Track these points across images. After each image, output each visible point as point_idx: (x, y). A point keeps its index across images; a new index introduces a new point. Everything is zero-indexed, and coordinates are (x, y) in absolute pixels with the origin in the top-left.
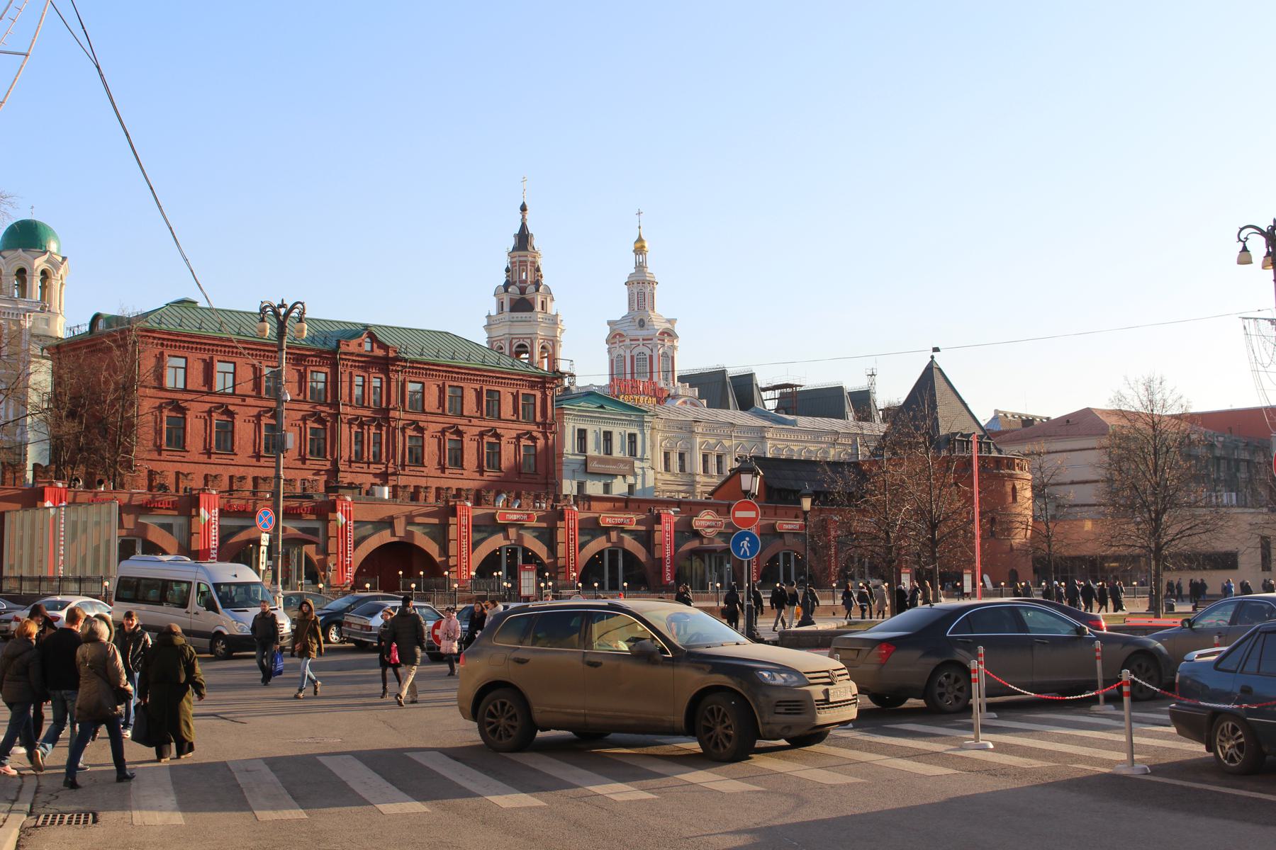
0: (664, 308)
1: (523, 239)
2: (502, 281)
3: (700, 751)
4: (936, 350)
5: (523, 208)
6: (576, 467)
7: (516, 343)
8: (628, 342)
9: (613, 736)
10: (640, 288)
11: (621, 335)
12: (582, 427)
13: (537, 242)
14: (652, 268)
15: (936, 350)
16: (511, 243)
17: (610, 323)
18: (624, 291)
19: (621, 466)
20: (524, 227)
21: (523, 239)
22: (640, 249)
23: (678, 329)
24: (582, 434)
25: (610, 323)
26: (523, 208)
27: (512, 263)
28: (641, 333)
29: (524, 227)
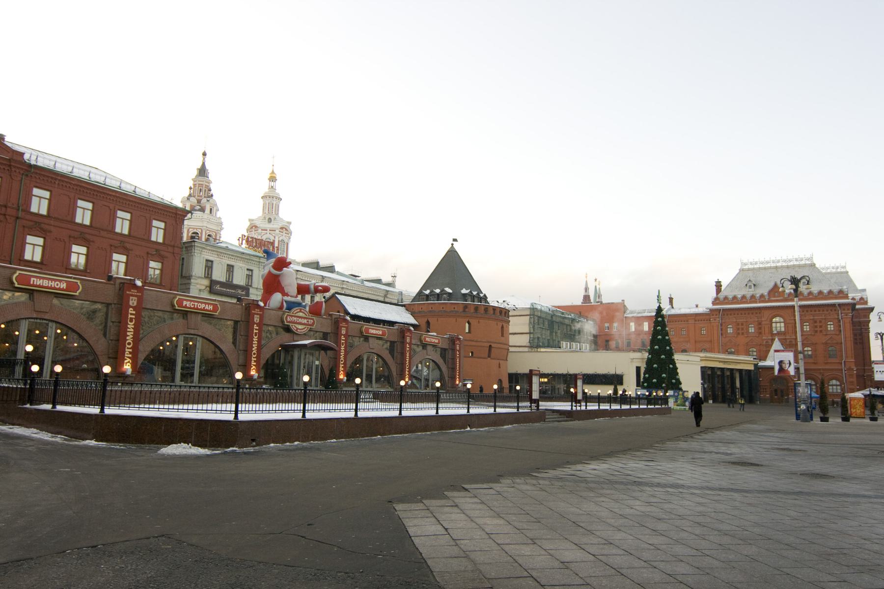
0: (285, 213)
1: (203, 171)
2: (187, 194)
3: (399, 507)
4: (455, 240)
5: (204, 154)
6: (204, 287)
7: (191, 231)
8: (260, 231)
9: (639, 513)
10: (271, 201)
11: (256, 227)
12: (211, 258)
13: (212, 176)
14: (281, 188)
15: (455, 240)
16: (195, 173)
17: (250, 220)
18: (261, 202)
19: (239, 291)
20: (204, 164)
21: (203, 171)
22: (273, 179)
23: (292, 227)
24: (209, 265)
25: (250, 220)
26: (204, 154)
27: (194, 185)
28: (270, 226)
29: (204, 164)
